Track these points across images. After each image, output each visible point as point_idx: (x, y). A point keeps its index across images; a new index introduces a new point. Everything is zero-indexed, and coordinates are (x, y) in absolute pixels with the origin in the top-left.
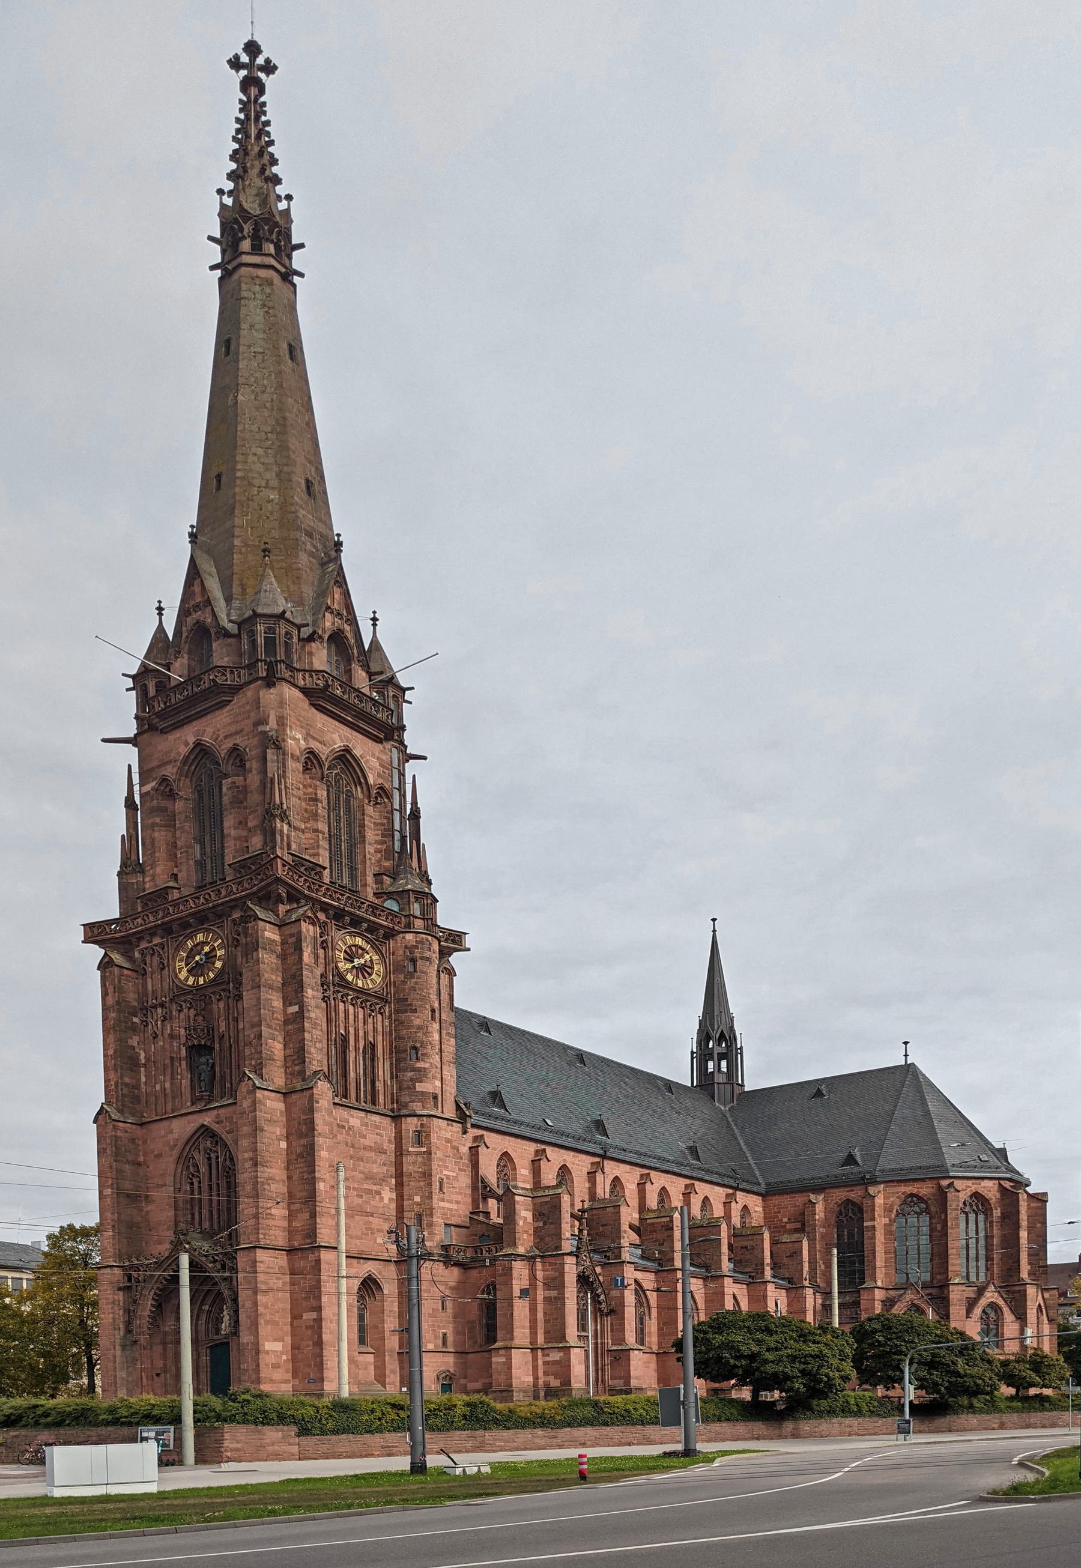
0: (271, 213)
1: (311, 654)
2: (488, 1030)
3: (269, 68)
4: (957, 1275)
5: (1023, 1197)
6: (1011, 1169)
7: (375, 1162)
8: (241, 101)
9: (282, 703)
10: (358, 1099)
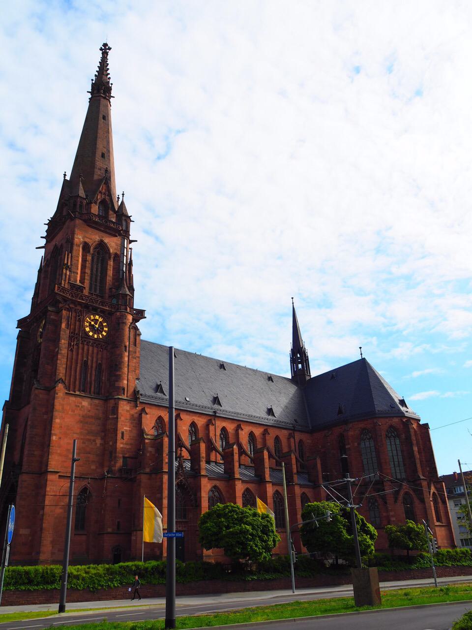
3: (110, 49)
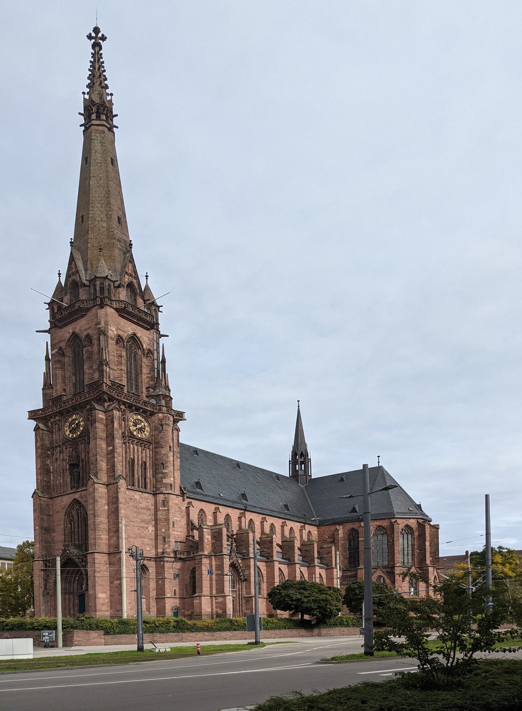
0: (104, 102)
1: (119, 293)
2: (197, 454)
3: (104, 38)
4: (399, 562)
5: (427, 526)
6: (423, 514)
7: (145, 514)
8: (92, 53)
9: (106, 315)
10: (139, 486)
